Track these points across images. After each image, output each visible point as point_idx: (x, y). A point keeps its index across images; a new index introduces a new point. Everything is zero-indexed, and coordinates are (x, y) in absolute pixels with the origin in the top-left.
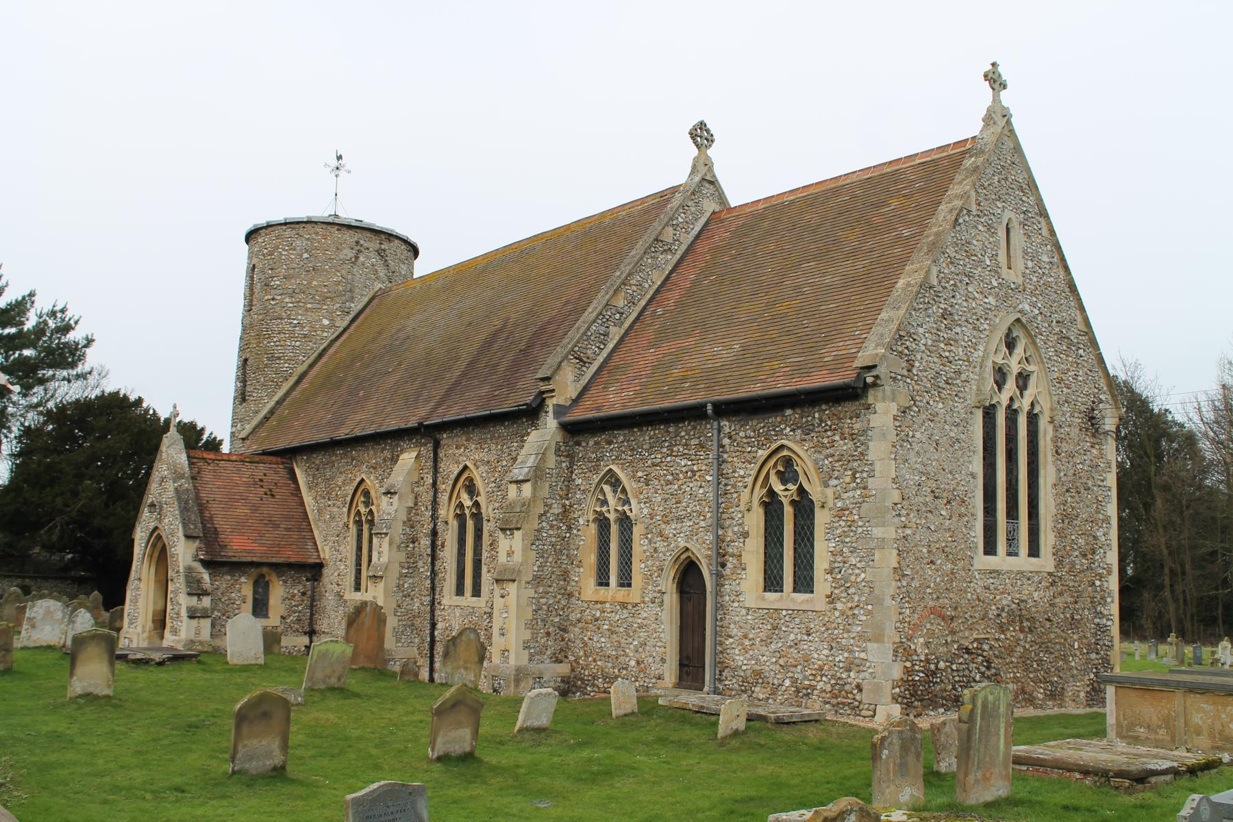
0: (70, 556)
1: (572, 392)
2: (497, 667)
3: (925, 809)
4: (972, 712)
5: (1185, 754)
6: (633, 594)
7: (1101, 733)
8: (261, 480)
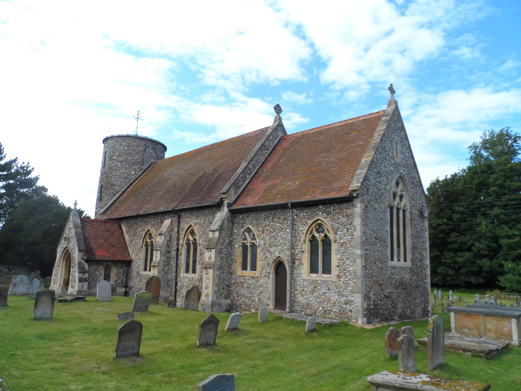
1: (233, 199)
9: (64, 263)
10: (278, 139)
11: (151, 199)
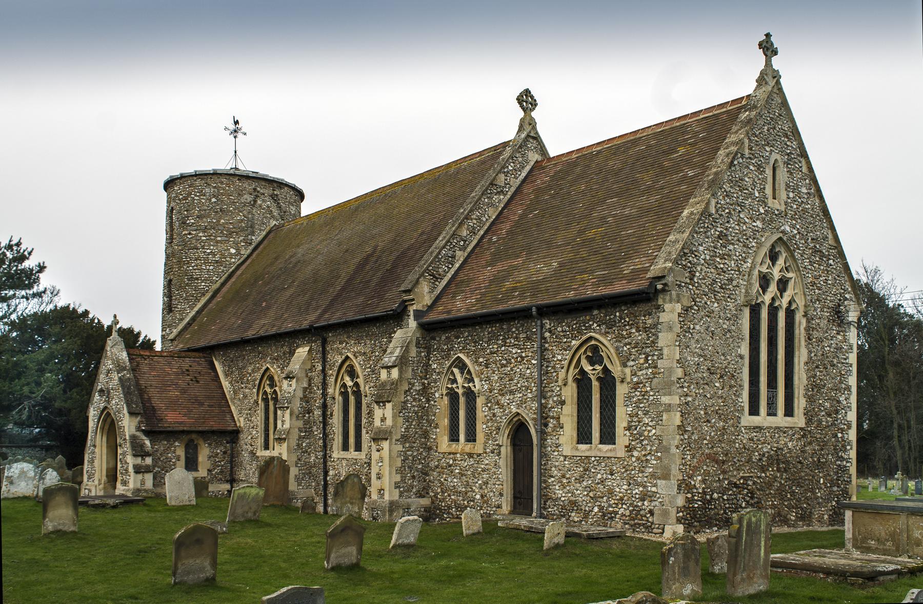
0: (37, 430)
1: (428, 300)
2: (375, 501)
3: (703, 599)
4: (739, 531)
5: (907, 560)
6: (478, 448)
7: (841, 545)
8: (188, 370)
9: (105, 439)
10: (528, 168)
11: (268, 307)
